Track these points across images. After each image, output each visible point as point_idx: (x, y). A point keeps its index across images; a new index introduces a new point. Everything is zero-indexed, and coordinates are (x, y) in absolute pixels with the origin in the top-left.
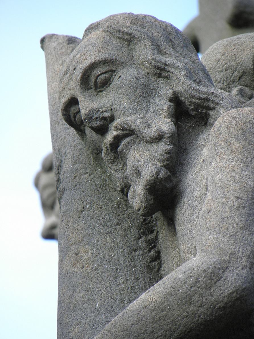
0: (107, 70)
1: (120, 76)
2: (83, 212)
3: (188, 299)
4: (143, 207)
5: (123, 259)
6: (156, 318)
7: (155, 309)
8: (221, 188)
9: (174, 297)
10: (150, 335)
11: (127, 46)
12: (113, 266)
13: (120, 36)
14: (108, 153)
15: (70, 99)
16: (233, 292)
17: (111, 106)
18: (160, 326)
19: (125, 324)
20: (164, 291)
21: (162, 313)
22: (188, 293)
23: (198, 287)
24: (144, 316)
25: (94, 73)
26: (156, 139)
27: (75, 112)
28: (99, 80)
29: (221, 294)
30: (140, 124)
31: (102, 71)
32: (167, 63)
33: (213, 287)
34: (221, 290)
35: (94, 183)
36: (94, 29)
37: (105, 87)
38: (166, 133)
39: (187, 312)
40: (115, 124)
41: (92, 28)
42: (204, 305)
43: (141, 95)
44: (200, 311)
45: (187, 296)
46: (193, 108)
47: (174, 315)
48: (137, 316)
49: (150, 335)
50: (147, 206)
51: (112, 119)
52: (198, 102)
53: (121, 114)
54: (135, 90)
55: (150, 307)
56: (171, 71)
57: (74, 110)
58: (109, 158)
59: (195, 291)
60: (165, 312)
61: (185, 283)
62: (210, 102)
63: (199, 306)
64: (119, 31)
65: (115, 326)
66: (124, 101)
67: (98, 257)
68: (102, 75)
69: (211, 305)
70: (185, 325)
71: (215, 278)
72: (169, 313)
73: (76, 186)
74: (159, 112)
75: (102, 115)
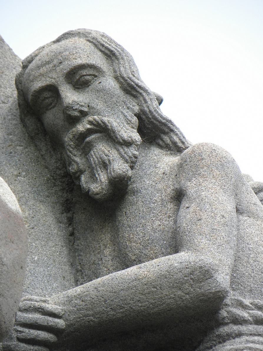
0: (92, 73)
1: (100, 82)
2: (19, 177)
3: (179, 285)
4: (103, 193)
5: (54, 227)
6: (146, 291)
8: (208, 204)
9: (168, 279)
10: (135, 303)
12: (46, 230)
13: (103, 49)
18: (147, 299)
22: (181, 280)
23: (191, 278)
24: (135, 286)
27: (46, 96)
29: (209, 289)
31: (88, 73)
33: (204, 282)
35: (28, 156)
40: (90, 118)
41: (73, 34)
42: (190, 294)
45: (179, 282)
47: (162, 294)
49: (135, 303)
56: (141, 92)
59: (187, 280)
61: (180, 272)
65: (103, 286)
67: (35, 218)
69: (196, 296)
70: (168, 305)
71: (208, 276)
73: (11, 153)
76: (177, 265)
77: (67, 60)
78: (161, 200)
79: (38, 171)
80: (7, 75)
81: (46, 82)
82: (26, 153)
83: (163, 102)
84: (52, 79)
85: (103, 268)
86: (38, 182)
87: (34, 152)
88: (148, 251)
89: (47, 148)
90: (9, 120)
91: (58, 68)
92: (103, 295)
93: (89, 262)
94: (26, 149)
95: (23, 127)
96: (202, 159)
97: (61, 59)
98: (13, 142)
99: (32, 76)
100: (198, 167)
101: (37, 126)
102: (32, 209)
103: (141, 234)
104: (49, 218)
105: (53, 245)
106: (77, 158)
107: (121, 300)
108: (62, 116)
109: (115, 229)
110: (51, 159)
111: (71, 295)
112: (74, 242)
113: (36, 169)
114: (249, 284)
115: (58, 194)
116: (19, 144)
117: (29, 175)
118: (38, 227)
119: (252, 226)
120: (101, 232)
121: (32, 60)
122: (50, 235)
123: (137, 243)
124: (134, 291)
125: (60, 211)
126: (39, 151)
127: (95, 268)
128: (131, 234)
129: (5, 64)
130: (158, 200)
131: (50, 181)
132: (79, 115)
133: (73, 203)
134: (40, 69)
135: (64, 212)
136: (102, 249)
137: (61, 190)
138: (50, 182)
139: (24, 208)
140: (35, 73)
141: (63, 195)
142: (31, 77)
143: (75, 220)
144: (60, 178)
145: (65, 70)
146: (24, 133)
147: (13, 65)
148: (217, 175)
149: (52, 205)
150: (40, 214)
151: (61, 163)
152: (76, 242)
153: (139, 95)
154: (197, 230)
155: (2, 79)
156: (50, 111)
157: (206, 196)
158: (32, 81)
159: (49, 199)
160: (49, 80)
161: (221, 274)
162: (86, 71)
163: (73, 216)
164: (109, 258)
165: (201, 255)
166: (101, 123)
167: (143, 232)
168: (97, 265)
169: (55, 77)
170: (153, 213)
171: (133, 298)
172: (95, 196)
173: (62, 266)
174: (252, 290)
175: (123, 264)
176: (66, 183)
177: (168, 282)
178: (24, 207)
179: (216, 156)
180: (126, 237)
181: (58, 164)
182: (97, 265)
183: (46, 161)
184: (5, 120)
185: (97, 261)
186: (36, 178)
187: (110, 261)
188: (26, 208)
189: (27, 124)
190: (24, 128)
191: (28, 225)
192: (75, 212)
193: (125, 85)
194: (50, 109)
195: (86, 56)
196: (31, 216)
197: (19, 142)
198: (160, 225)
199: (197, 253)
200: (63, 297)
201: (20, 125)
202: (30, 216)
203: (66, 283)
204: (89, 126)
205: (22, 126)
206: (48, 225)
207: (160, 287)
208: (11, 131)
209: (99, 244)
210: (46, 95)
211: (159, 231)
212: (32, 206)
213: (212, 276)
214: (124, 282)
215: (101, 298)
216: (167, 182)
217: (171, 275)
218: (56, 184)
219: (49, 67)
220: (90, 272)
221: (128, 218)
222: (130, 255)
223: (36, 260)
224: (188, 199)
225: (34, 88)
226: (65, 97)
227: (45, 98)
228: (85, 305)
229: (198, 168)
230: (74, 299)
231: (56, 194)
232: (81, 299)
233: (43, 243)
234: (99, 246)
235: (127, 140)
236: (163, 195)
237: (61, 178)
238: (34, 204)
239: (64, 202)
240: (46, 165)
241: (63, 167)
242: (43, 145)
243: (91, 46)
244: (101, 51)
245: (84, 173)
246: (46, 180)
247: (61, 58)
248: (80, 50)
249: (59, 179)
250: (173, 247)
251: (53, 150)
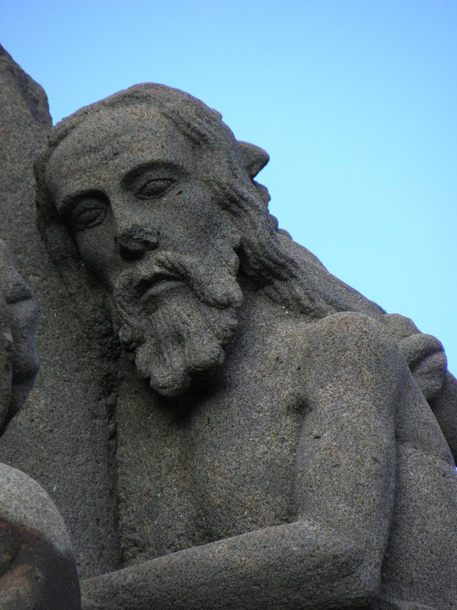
1: (180, 193)
4: (175, 388)
7: (244, 577)
11: (191, 149)
13: (188, 132)
14: (128, 287)
15: (92, 191)
16: (363, 598)
17: (160, 228)
19: (189, 578)
20: (265, 559)
21: (253, 587)
24: (224, 580)
25: (149, 174)
26: (223, 305)
27: (88, 207)
28: (151, 186)
30: (204, 275)
31: (161, 177)
32: (245, 197)
34: (348, 588)
36: (140, 100)
37: (152, 197)
38: (235, 301)
39: (289, 599)
40: (161, 255)
41: (137, 98)
42: (315, 599)
43: (203, 229)
44: (306, 603)
46: (257, 268)
48: (214, 576)
49: (222, 607)
50: (180, 389)
51: (155, 247)
52: (271, 265)
53: (170, 245)
54: (198, 220)
55: (237, 572)
56: (246, 208)
57: (88, 204)
58: (127, 294)
60: (258, 588)
61: (301, 561)
62: (285, 271)
63: (308, 598)
64: (189, 125)
66: (179, 229)
68: (159, 181)
69: (324, 602)
71: (346, 571)
72: (264, 591)
74: (221, 262)
75: (146, 237)
76: (296, 549)
77: (128, 150)
78: (271, 409)
79: (63, 324)
80: (17, 138)
81: (89, 185)
82: (43, 290)
83: (269, 163)
84: (100, 181)
85: (164, 506)
86: (62, 344)
87: (58, 287)
88: (244, 495)
89: (79, 283)
90: (18, 225)
91: (111, 163)
92: (170, 590)
93: (139, 489)
94: (44, 281)
95: (41, 240)
96: (346, 350)
97: (118, 148)
98: (22, 267)
99: (64, 168)
100: (338, 363)
101: (66, 244)
102: (51, 395)
103: (234, 463)
104: (79, 411)
105: (82, 461)
106: (133, 318)
107: (200, 601)
108: (113, 244)
109: (188, 441)
110: (86, 303)
111: (117, 585)
112: (116, 449)
113: (60, 320)
114: (409, 572)
115: (93, 364)
116: (33, 272)
117: (48, 332)
118: (59, 430)
119: (420, 467)
120: (163, 442)
121: (65, 134)
122: (78, 444)
123: (226, 478)
124: (222, 587)
125: (96, 396)
126: (66, 286)
127: (150, 502)
128: (217, 461)
129: (14, 116)
130: (266, 408)
131: (81, 341)
132: (141, 248)
133: (117, 379)
134: (79, 158)
135: (102, 396)
136: (163, 472)
137: (100, 358)
138: (82, 343)
139: (38, 394)
140: (71, 164)
141: (102, 366)
142: (64, 170)
143: (118, 409)
144: (98, 337)
145: (123, 168)
146: (42, 251)
147: (26, 118)
148: (368, 381)
149: (84, 385)
150: (63, 404)
151: (102, 313)
152: (119, 449)
153: (243, 213)
154: (332, 485)
155: (8, 145)
156: (92, 229)
157: (348, 421)
158: (64, 177)
159: (79, 374)
160: (95, 181)
161: (367, 566)
162: (158, 173)
163: (116, 402)
164: (174, 490)
165: (336, 534)
166: (179, 267)
167: (237, 460)
168: (153, 499)
169: (108, 179)
170: (256, 430)
171: (220, 600)
172: (160, 390)
173: (95, 499)
174: (414, 583)
175: (198, 507)
176: (109, 346)
177: (279, 577)
178: (38, 392)
179: (369, 345)
180: (207, 463)
181: (97, 314)
182: (153, 499)
183: (77, 306)
184: (11, 224)
185: (155, 492)
186: (60, 336)
187: (177, 496)
188: (42, 393)
189: (49, 239)
190: (43, 242)
191: (45, 424)
192: (120, 395)
193: (221, 197)
194: (93, 227)
195: (160, 146)
196: (49, 408)
197: (33, 269)
198: (266, 453)
199: (330, 530)
200: (103, 586)
201: (35, 235)
202: (47, 408)
203: (102, 530)
204: (157, 269)
205: (40, 239)
206: (76, 424)
207: (267, 585)
208: (20, 246)
209: (158, 462)
210: (88, 204)
211: (264, 464)
212: (51, 389)
213: (353, 572)
214: (207, 572)
215: (167, 594)
216: (282, 377)
217: (286, 567)
218: (91, 347)
219: (96, 159)
220: (140, 507)
221: (212, 430)
222: (212, 495)
223: (54, 491)
224: (318, 420)
225: (68, 191)
226: (120, 218)
227: (85, 208)
228: (139, 604)
229: (338, 365)
230: (121, 591)
231: (90, 365)
232: (134, 592)
233: (66, 459)
234: (159, 467)
235: (220, 300)
236: (274, 400)
237: (100, 338)
238: (55, 387)
239: (103, 379)
240: (76, 312)
241: (106, 319)
242: (75, 278)
243: (168, 125)
244: (184, 134)
245: (143, 345)
246: (76, 339)
247: (117, 146)
248: (150, 135)
249: (98, 338)
250: (286, 495)
251: (90, 288)
